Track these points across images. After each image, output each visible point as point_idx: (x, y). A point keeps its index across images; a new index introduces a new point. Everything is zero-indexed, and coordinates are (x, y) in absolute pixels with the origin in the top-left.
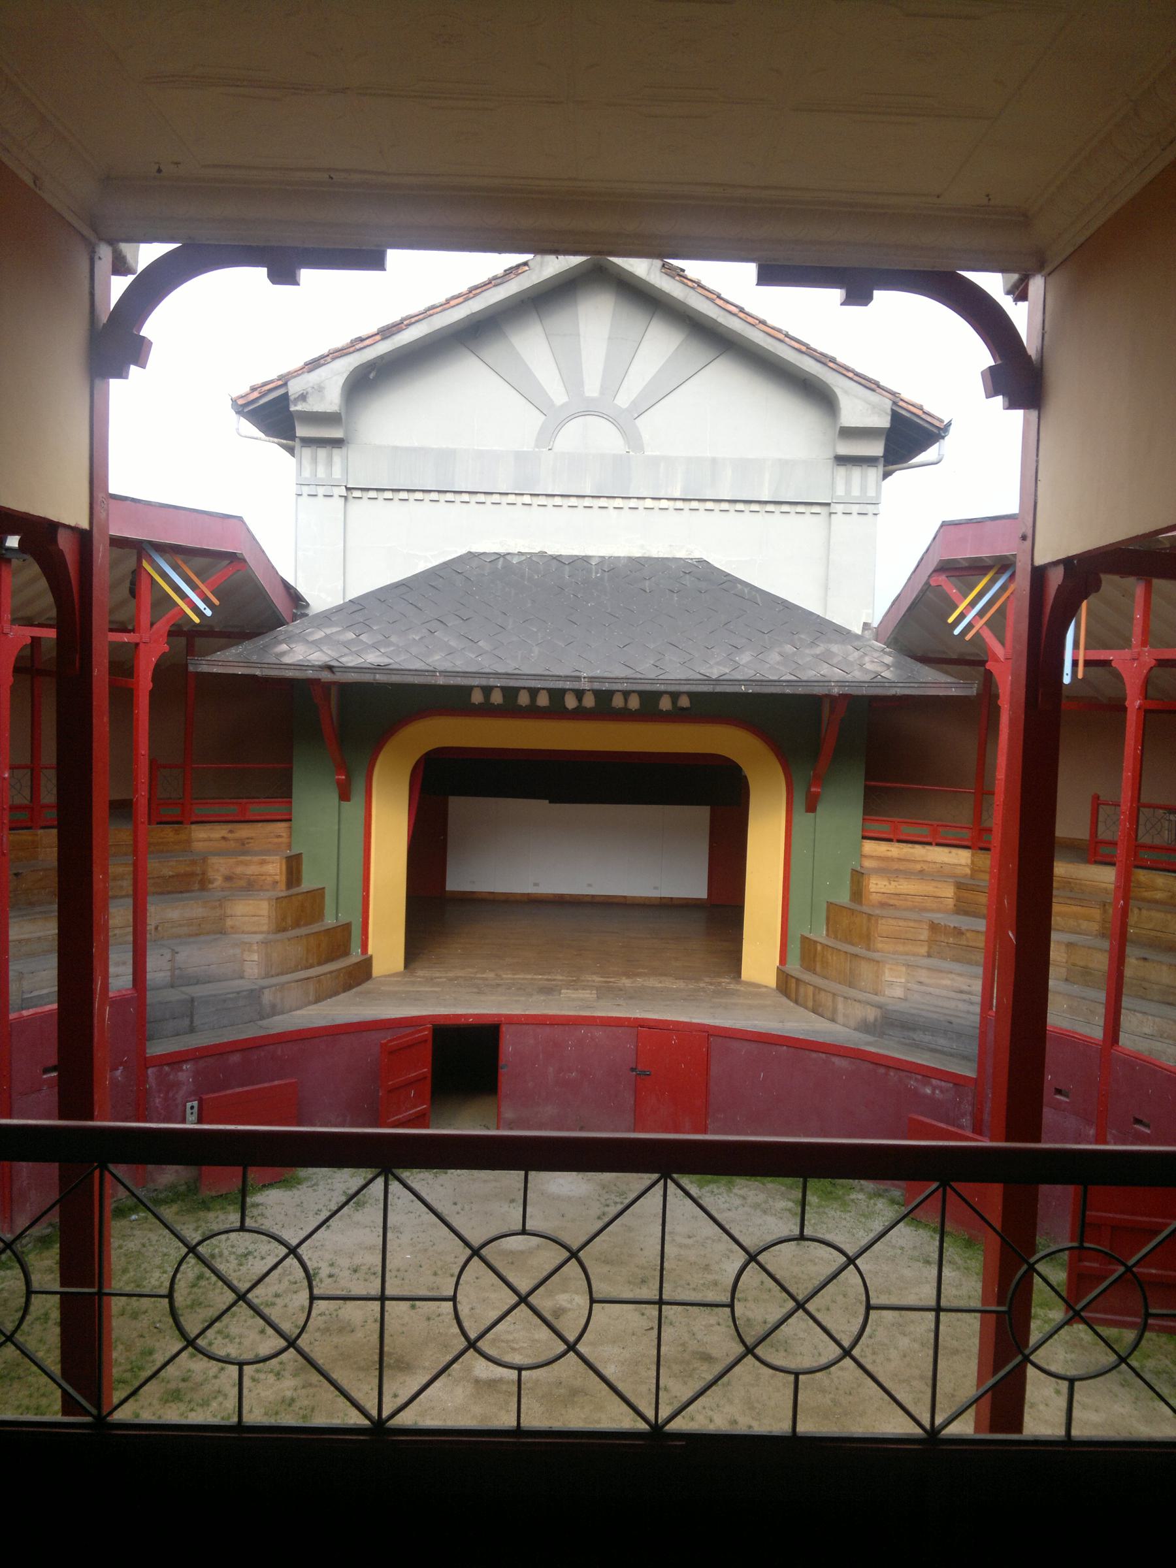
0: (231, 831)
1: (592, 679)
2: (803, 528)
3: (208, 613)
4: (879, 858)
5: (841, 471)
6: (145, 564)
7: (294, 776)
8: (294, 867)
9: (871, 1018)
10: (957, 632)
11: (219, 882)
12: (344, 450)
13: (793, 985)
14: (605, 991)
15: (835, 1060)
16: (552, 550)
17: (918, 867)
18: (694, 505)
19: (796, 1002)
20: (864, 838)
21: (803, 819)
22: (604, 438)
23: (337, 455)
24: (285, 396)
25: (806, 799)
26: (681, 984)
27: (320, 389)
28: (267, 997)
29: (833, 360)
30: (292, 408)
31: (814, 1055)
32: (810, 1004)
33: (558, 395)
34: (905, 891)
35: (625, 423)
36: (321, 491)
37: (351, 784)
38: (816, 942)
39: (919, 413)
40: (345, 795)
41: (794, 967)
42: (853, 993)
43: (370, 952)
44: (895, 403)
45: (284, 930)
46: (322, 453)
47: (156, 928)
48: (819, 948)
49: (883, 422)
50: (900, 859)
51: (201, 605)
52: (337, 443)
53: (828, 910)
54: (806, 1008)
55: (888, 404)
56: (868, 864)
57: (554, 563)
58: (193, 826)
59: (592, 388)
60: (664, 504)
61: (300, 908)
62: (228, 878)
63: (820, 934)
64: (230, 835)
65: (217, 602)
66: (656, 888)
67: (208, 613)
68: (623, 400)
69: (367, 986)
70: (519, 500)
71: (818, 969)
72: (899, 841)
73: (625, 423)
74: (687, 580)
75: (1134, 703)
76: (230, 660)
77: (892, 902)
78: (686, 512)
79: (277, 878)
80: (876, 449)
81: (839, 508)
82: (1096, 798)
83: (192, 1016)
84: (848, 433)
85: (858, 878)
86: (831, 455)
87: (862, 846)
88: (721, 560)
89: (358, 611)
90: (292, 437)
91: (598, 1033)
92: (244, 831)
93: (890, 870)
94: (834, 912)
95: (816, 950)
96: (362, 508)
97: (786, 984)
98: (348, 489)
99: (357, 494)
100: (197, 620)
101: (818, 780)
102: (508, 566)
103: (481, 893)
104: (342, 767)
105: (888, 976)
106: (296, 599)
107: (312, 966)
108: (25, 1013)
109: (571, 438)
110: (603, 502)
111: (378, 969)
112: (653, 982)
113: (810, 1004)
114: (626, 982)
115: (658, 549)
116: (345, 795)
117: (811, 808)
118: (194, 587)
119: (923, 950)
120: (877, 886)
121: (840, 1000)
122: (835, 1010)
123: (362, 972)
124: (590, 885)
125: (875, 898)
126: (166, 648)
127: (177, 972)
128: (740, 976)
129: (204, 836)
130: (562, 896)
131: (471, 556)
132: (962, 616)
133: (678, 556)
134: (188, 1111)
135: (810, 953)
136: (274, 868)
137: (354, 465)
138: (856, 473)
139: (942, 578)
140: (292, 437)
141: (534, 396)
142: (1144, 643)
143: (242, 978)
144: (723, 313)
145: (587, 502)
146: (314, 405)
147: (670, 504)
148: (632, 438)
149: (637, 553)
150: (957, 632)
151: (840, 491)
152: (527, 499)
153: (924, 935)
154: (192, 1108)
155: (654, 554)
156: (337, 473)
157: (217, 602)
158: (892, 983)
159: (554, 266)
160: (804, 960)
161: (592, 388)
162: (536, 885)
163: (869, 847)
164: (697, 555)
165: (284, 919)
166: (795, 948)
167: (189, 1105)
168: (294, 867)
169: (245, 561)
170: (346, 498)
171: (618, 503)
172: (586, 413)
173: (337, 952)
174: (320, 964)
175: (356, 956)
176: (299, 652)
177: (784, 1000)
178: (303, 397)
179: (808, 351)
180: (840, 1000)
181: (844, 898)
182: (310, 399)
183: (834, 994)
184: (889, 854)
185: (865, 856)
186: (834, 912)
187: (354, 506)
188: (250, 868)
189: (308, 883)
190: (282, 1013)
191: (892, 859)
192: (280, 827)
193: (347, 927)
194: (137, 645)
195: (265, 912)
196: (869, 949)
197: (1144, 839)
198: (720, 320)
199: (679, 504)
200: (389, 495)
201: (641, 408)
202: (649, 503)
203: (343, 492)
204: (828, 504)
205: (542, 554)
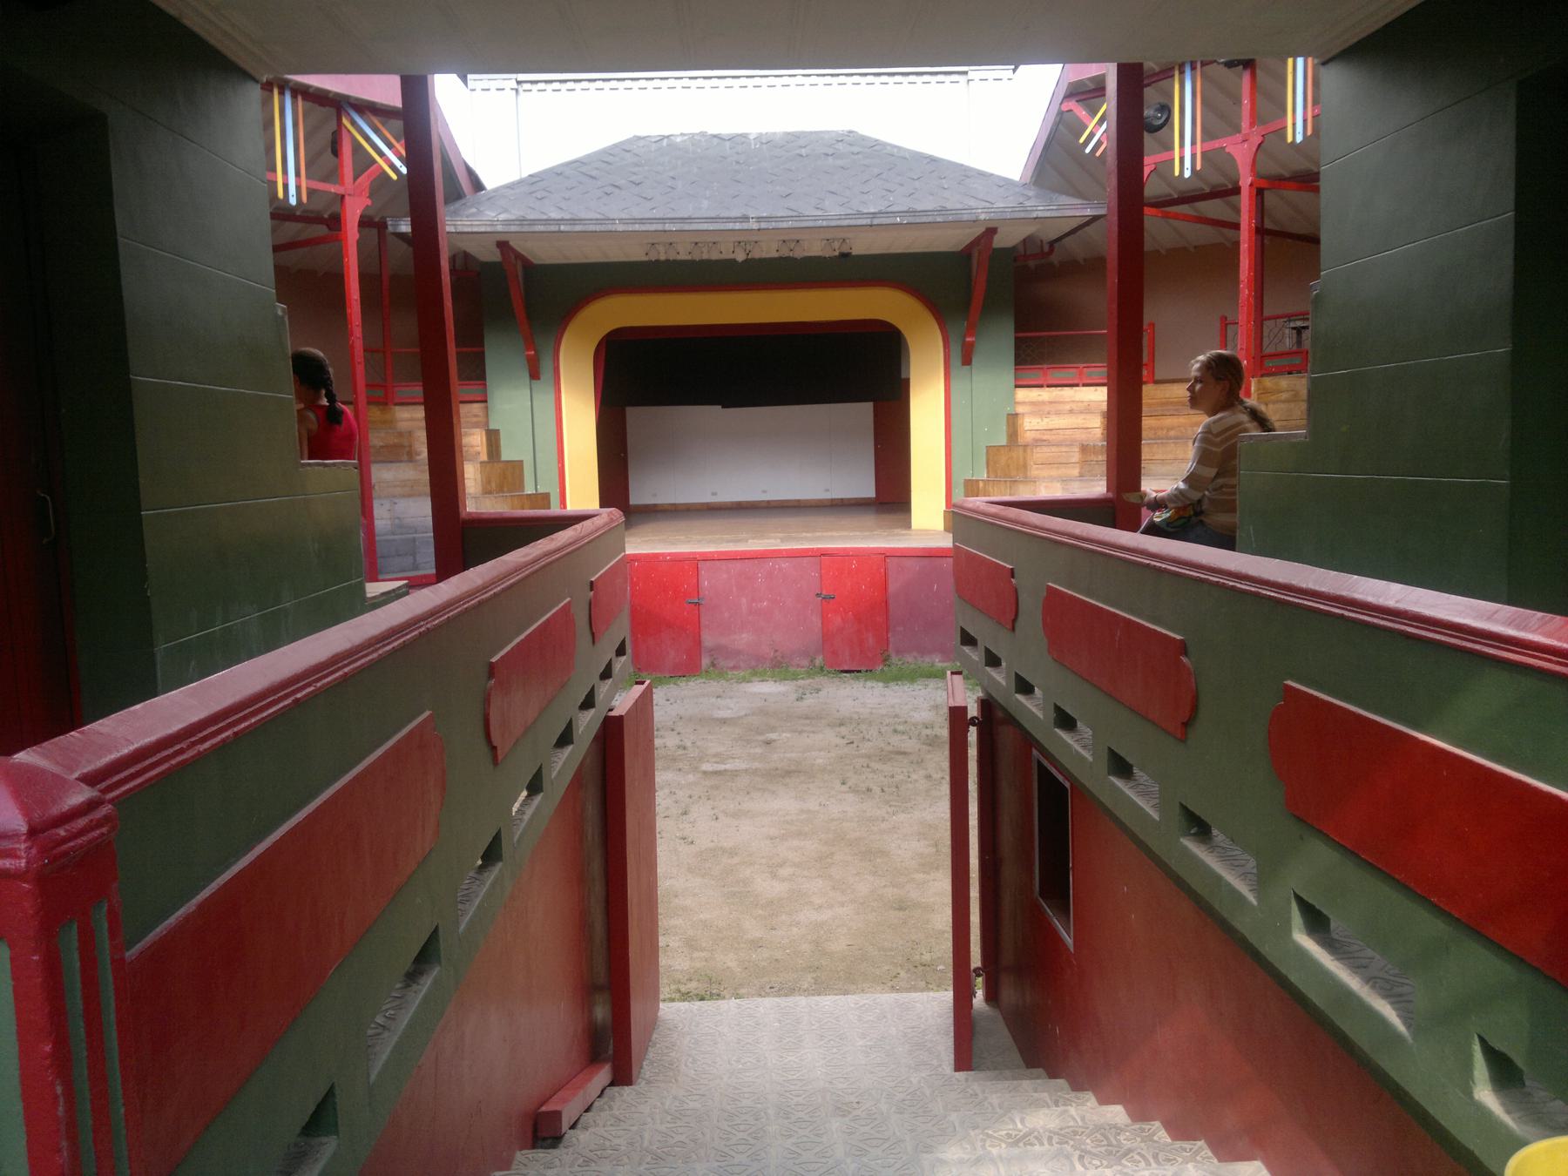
1: (759, 219)
4: (1033, 403)
7: (488, 361)
10: (1088, 150)
14: (782, 540)
17: (1068, 407)
21: (958, 370)
40: (535, 375)
56: (1020, 409)
57: (716, 141)
58: (397, 408)
74: (840, 146)
75: (1246, 181)
82: (1224, 319)
83: (414, 555)
85: (1013, 419)
87: (1014, 395)
89: (535, 184)
91: (785, 564)
93: (1039, 409)
101: (971, 330)
102: (673, 146)
104: (530, 343)
106: (478, 185)
117: (967, 361)
119: (1076, 472)
120: (1031, 425)
125: (1029, 436)
126: (369, 202)
132: (1092, 135)
139: (1072, 104)
142: (1252, 124)
150: (1088, 150)
153: (1076, 456)
159: (543, 1109)
163: (1022, 394)
165: (489, 482)
181: (1002, 440)
189: (506, 455)
191: (1043, 403)
194: (343, 197)
197: (1268, 349)
205: (703, 134)
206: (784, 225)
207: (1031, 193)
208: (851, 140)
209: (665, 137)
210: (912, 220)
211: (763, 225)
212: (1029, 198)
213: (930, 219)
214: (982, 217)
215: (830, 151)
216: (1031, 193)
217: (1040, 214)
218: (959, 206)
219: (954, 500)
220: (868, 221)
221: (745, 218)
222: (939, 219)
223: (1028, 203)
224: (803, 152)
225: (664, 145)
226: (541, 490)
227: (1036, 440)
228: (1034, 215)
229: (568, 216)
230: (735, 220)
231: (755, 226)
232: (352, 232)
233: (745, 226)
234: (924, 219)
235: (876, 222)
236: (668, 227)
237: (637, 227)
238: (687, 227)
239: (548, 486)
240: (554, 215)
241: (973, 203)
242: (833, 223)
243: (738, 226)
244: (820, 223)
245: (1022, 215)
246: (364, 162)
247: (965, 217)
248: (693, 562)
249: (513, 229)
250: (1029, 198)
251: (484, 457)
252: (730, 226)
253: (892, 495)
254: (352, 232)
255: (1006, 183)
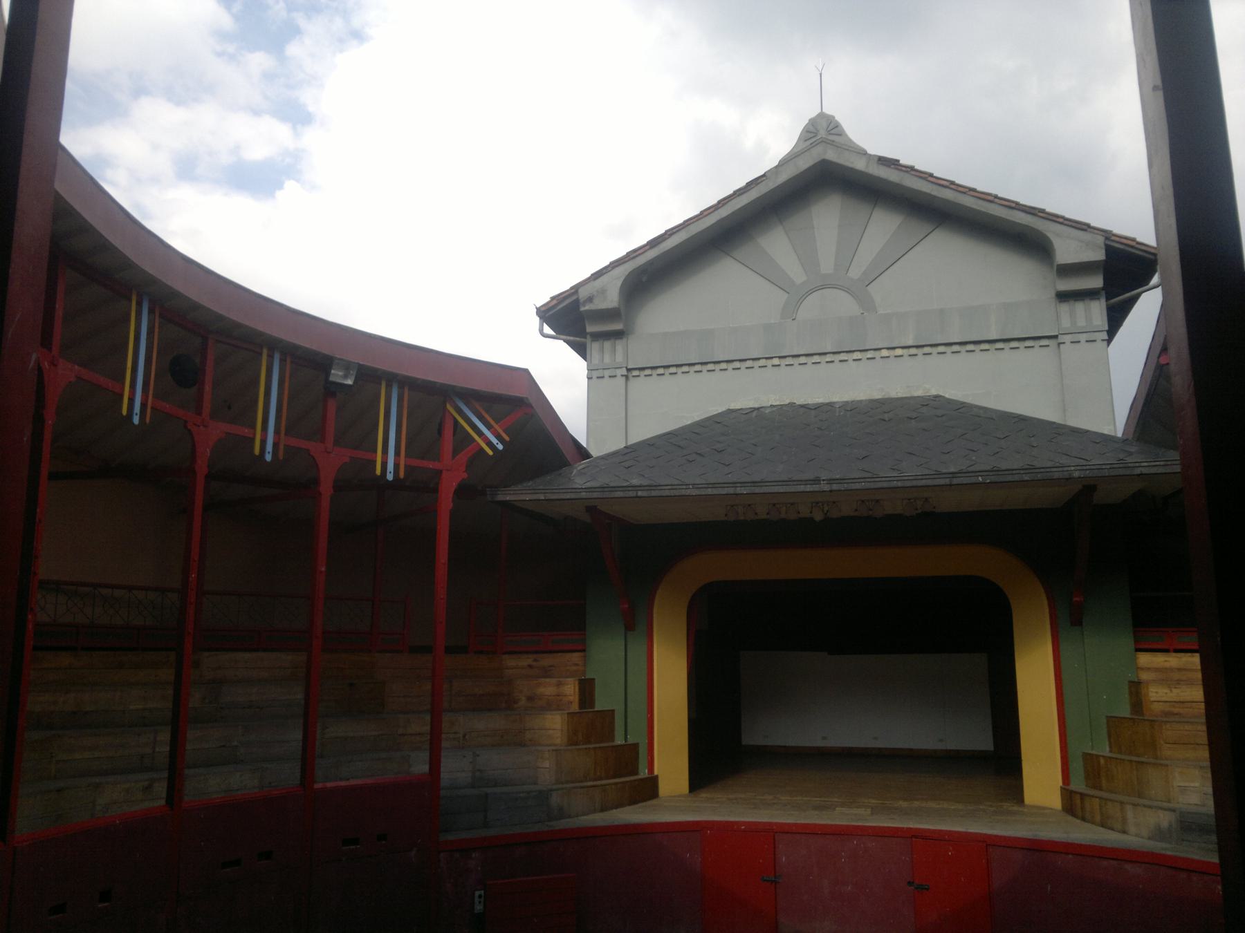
0: (535, 660)
1: (831, 481)
2: (1037, 358)
3: (500, 447)
4: (1157, 670)
5: (1064, 308)
6: (449, 407)
8: (587, 689)
9: (1165, 824)
11: (523, 702)
12: (624, 340)
13: (1078, 802)
15: (1128, 867)
16: (800, 401)
18: (927, 350)
19: (1083, 819)
20: (1138, 650)
22: (843, 304)
23: (620, 345)
24: (577, 301)
25: (1069, 619)
26: (960, 806)
27: (603, 292)
28: (555, 800)
29: (1043, 211)
30: (582, 309)
31: (1105, 863)
32: (1098, 818)
33: (796, 273)
34: (1189, 699)
35: (859, 291)
36: (607, 373)
37: (635, 622)
38: (1098, 756)
39: (1133, 244)
40: (630, 627)
41: (1078, 785)
42: (1142, 801)
43: (656, 773)
44: (1107, 238)
45: (576, 744)
46: (607, 345)
47: (464, 736)
48: (1102, 761)
49: (1100, 255)
50: (1179, 670)
51: (494, 440)
52: (619, 335)
53: (1108, 727)
54: (1093, 823)
55: (1100, 240)
56: (1144, 676)
59: (827, 265)
60: (899, 352)
61: (592, 725)
62: (530, 699)
63: (1104, 749)
64: (534, 664)
65: (507, 438)
66: (941, 740)
67: (500, 447)
68: (855, 272)
69: (654, 802)
70: (770, 363)
71: (1104, 783)
72: (1176, 651)
73: (859, 291)
76: (521, 494)
77: (1176, 710)
78: (920, 357)
79: (571, 698)
80: (1097, 282)
81: (1067, 339)
84: (1066, 271)
85: (1136, 687)
86: (1053, 294)
88: (953, 393)
90: (582, 333)
92: (547, 660)
94: (1114, 723)
95: (1099, 763)
96: (640, 385)
97: (1072, 804)
98: (629, 370)
99: (635, 373)
100: (491, 453)
103: (772, 747)
105: (1178, 781)
107: (601, 779)
108: (329, 785)
109: (811, 308)
110: (843, 356)
111: (664, 789)
112: (932, 805)
113: (1098, 818)
114: (904, 804)
115: (897, 390)
116: (630, 627)
118: (489, 427)
120: (1157, 694)
121: (1129, 807)
122: (1124, 821)
123: (648, 790)
124: (876, 738)
125: (1157, 708)
126: (465, 475)
127: (478, 774)
128: (1022, 801)
129: (515, 664)
130: (850, 749)
131: (730, 411)
133: (916, 394)
134: (477, 900)
135: (1095, 770)
136: (571, 689)
137: (637, 350)
138: (1080, 307)
140: (582, 333)
141: (777, 279)
143: (535, 784)
144: (935, 187)
145: (828, 358)
146: (599, 305)
147: (905, 352)
148: (867, 304)
149: (877, 395)
151: (1066, 323)
152: (776, 361)
154: (480, 896)
155: (893, 395)
156: (619, 358)
157: (507, 438)
158: (1183, 790)
160: (1088, 782)
161: (827, 265)
162: (824, 738)
163: (1144, 659)
164: (934, 392)
166: (1077, 767)
167: (477, 893)
168: (587, 689)
169: (530, 406)
170: (627, 377)
171: (857, 355)
172: (823, 287)
173: (628, 771)
174: (608, 778)
175: (644, 773)
176: (579, 480)
177: (1070, 818)
178: (590, 299)
179: (1017, 206)
180: (1129, 807)
181: (1125, 711)
182: (596, 301)
183: (1122, 803)
184: (1167, 665)
185: (1142, 669)
186: (1114, 723)
187: (633, 383)
188: (547, 689)
190: (570, 817)
191: (1171, 670)
192: (576, 657)
193: (635, 747)
195: (558, 726)
196: (1157, 758)
198: (934, 193)
199: (913, 351)
200: (661, 371)
201: (872, 276)
202: (885, 353)
203: (624, 372)
204: (1056, 337)
205: (792, 405)
206: (857, 486)
207: (1133, 449)
208: (937, 402)
209: (755, 409)
210: (994, 479)
211: (835, 487)
212: (1131, 454)
213: (1016, 478)
214: (1076, 474)
215: (915, 415)
216: (1133, 449)
217: (1145, 471)
218: (1049, 464)
219: (1073, 787)
220: (947, 481)
221: (817, 481)
222: (1026, 478)
223: (1129, 460)
224: (886, 417)
225: (755, 416)
226: (631, 740)
227: (1167, 714)
228: (1138, 471)
229: (645, 482)
230: (806, 482)
231: (827, 488)
232: (446, 502)
233: (816, 488)
234: (1010, 478)
235: (955, 481)
236: (739, 490)
237: (709, 491)
238: (757, 490)
239: (636, 736)
240: (635, 482)
241: (1064, 460)
242: (908, 484)
243: (809, 488)
244: (895, 484)
245: (1121, 472)
246: (463, 440)
247: (1056, 476)
248: (770, 833)
249: (595, 495)
250: (1131, 454)
251: (575, 707)
252: (801, 488)
253: (1002, 763)
254: (446, 502)
255: (1107, 439)
